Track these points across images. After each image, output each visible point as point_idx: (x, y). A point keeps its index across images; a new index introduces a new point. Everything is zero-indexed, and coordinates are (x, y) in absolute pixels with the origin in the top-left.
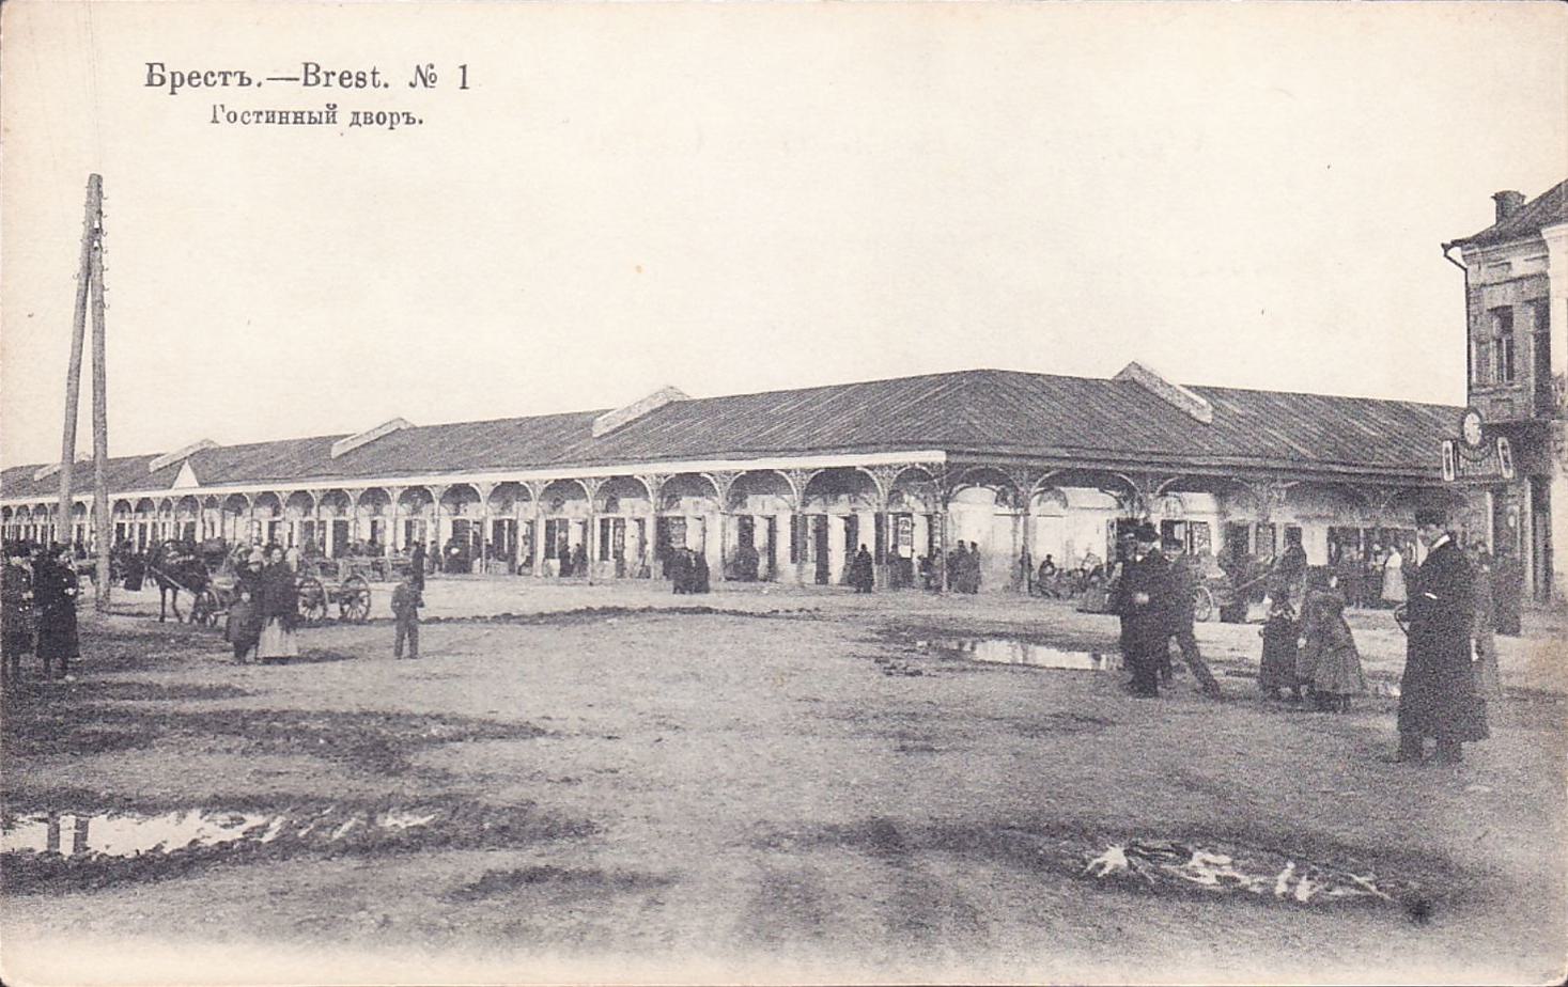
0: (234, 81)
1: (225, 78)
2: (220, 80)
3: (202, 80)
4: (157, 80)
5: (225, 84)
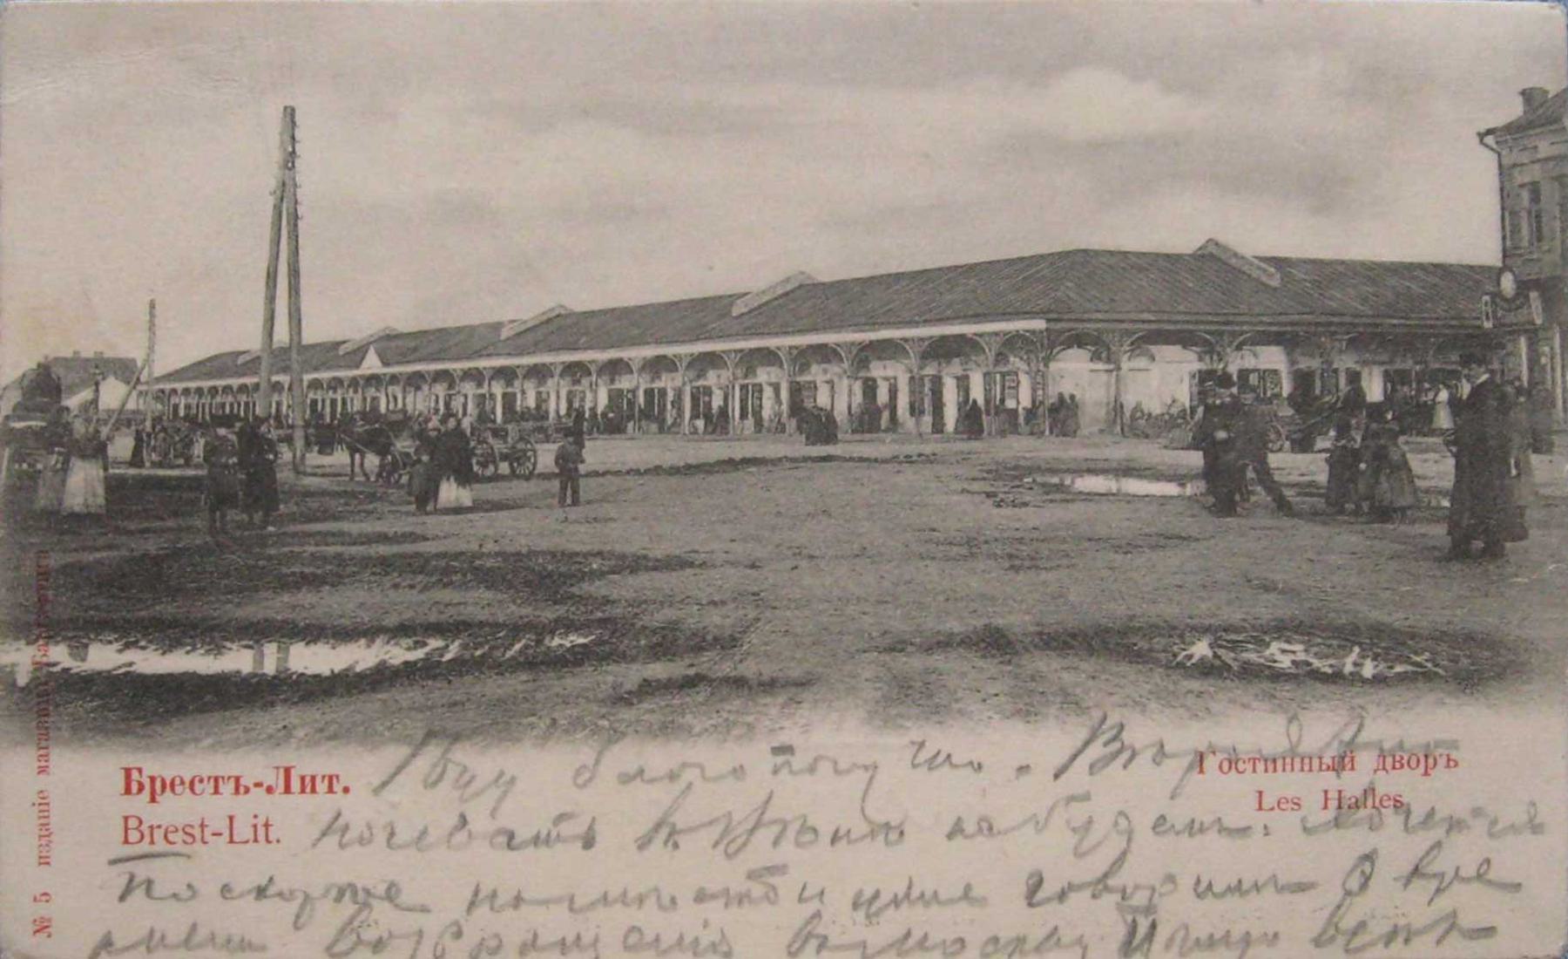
4: (135, 787)
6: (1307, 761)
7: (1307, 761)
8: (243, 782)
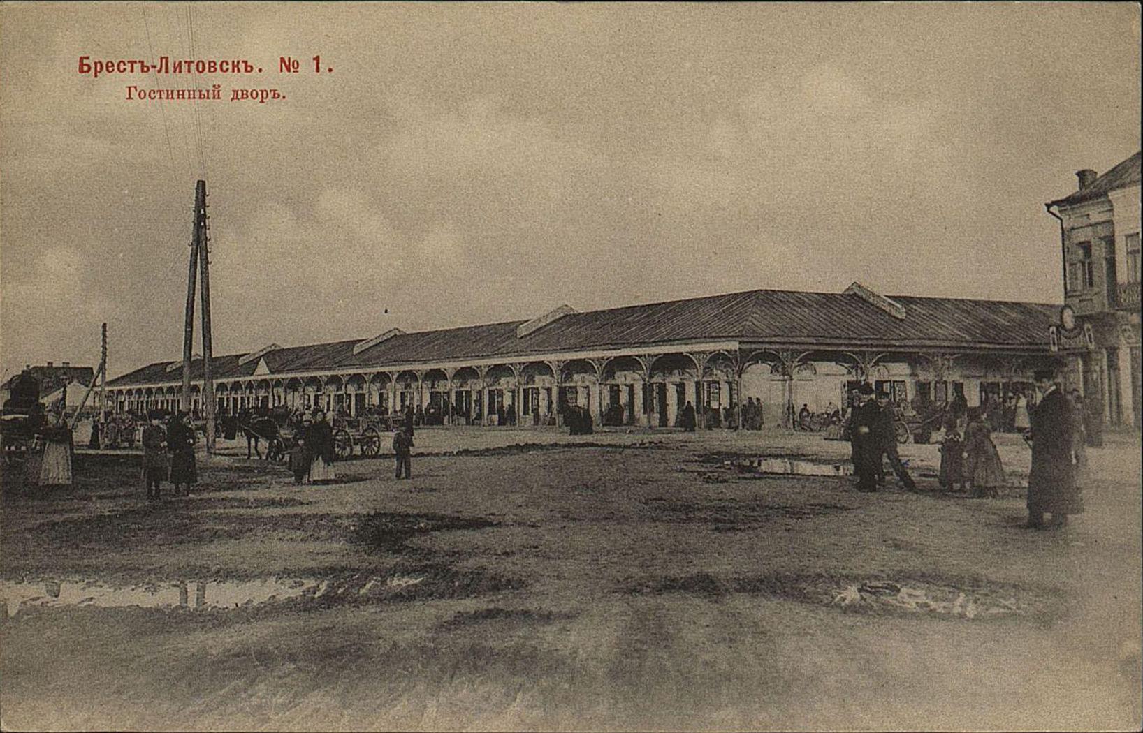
0: (137, 67)
1: (189, 66)
2: (128, 67)
3: (116, 67)
4: (85, 68)
5: (132, 71)
6: (164, 60)
7: (164, 60)
8: (249, 64)
